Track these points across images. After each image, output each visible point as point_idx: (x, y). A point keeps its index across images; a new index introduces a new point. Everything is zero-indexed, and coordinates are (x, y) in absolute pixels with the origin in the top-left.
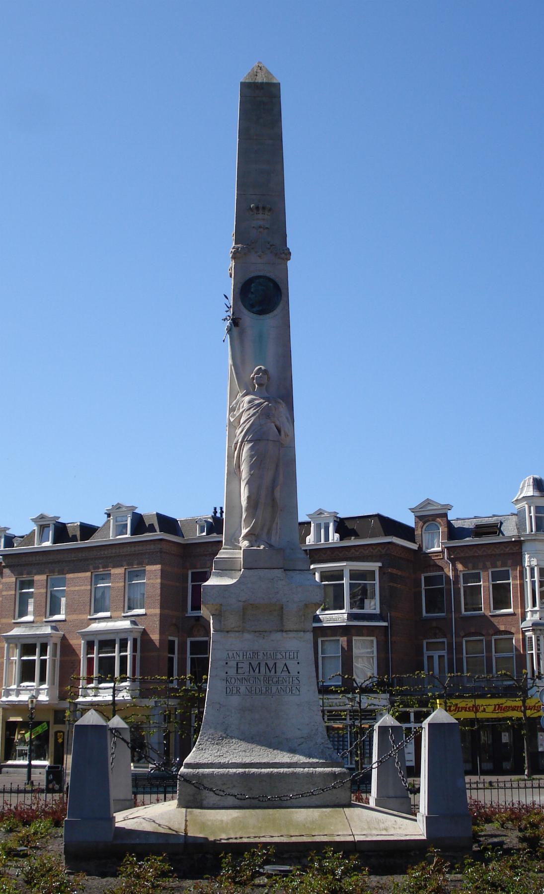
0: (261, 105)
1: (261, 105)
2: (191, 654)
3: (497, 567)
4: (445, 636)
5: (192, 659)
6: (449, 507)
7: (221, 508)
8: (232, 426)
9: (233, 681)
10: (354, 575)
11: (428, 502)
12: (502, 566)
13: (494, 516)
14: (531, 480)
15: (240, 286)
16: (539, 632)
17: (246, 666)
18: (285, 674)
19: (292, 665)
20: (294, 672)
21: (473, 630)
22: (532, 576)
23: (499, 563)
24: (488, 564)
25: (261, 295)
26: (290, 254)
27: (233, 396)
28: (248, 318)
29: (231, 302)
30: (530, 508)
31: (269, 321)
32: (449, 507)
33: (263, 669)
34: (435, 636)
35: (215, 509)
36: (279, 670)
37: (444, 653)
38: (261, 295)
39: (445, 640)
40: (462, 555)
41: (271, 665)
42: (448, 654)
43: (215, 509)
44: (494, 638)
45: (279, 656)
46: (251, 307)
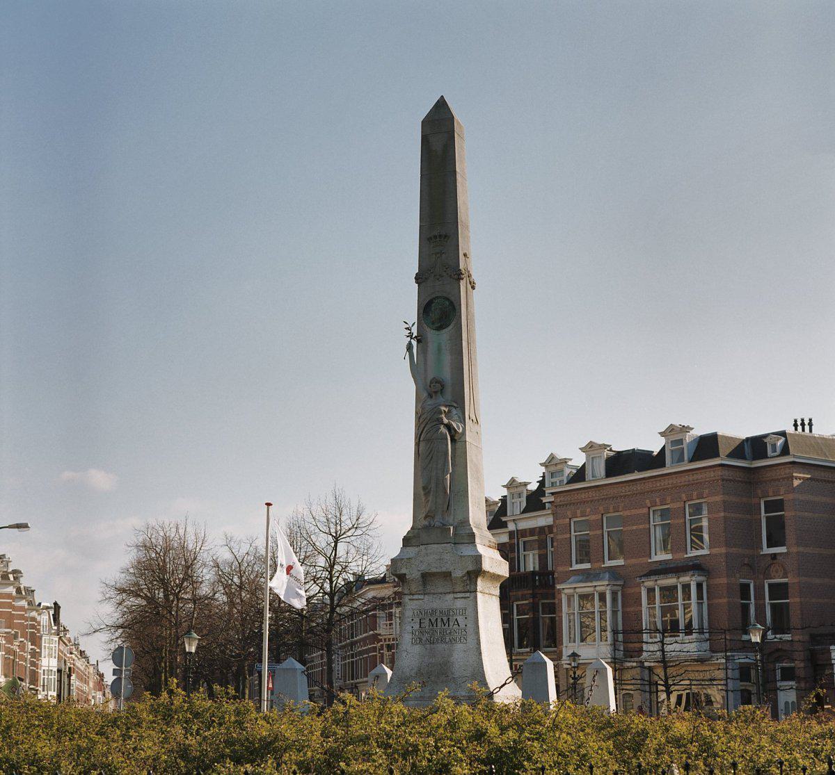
0: (439, 131)
1: (439, 131)
2: (766, 512)
5: (767, 517)
7: (803, 420)
9: (417, 633)
10: (575, 532)
15: (423, 306)
17: (427, 622)
19: (460, 619)
20: (462, 626)
26: (415, 278)
28: (431, 334)
31: (446, 334)
33: (439, 624)
35: (796, 421)
36: (451, 624)
41: (445, 619)
43: (796, 421)
45: (451, 613)
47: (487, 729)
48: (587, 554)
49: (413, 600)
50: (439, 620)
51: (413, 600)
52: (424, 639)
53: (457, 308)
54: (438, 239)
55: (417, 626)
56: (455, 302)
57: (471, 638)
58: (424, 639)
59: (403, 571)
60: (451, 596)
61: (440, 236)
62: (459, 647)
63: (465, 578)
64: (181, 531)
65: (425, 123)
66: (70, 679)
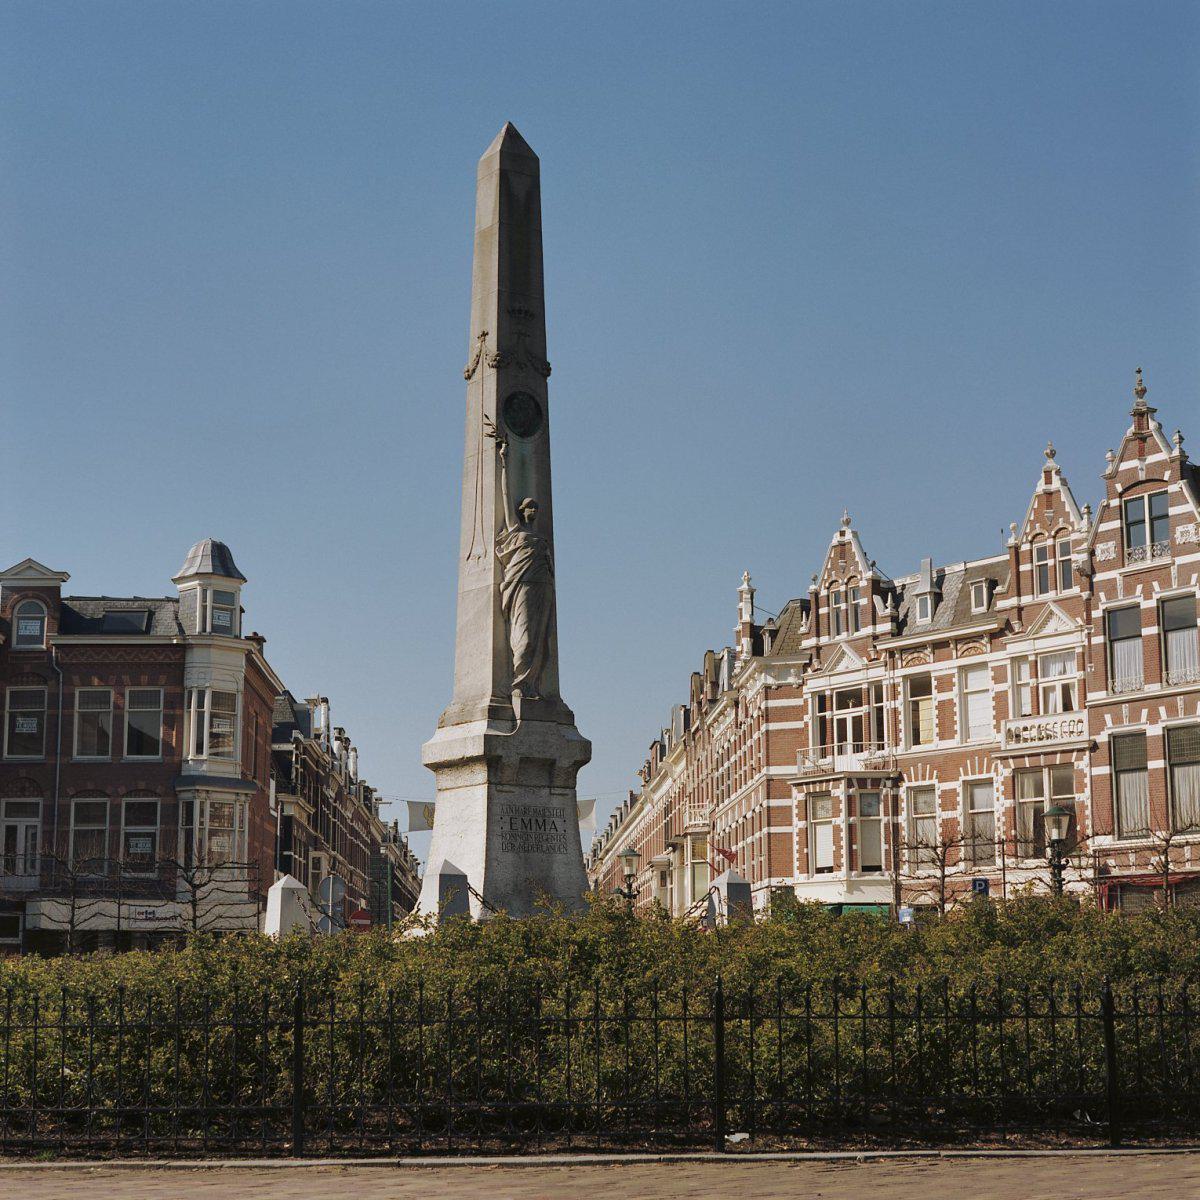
0: (520, 171)
1: (520, 171)
3: (139, 684)
4: (41, 794)
6: (63, 577)
8: (501, 564)
11: (29, 564)
12: (149, 684)
13: (136, 599)
14: (209, 546)
16: (243, 798)
18: (553, 831)
19: (558, 822)
21: (90, 786)
22: (201, 704)
23: (144, 678)
24: (126, 678)
25: (523, 415)
27: (500, 527)
29: (493, 419)
30: (204, 592)
32: (63, 577)
33: (534, 828)
34: (23, 792)
37: (36, 821)
38: (523, 415)
39: (40, 800)
40: (83, 660)
41: (540, 820)
42: (44, 823)
44: (125, 801)
46: (513, 426)
47: (1152, 951)
48: (550, 765)
49: (502, 791)
50: (533, 822)
51: (502, 791)
52: (517, 845)
53: (544, 413)
54: (522, 315)
55: (507, 828)
56: (541, 405)
57: (571, 847)
58: (517, 845)
59: (499, 752)
60: (547, 790)
61: (526, 312)
62: (559, 857)
63: (570, 770)
64: (191, 665)
65: (535, 160)
66: (144, 836)
